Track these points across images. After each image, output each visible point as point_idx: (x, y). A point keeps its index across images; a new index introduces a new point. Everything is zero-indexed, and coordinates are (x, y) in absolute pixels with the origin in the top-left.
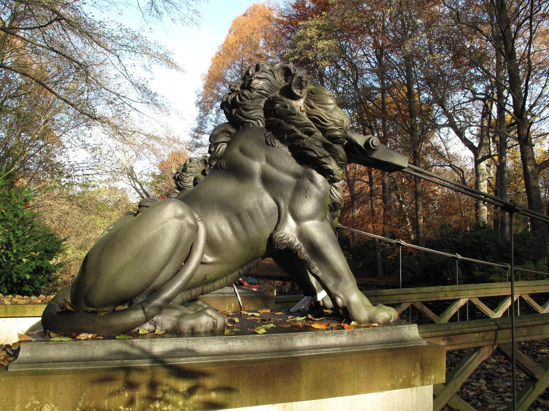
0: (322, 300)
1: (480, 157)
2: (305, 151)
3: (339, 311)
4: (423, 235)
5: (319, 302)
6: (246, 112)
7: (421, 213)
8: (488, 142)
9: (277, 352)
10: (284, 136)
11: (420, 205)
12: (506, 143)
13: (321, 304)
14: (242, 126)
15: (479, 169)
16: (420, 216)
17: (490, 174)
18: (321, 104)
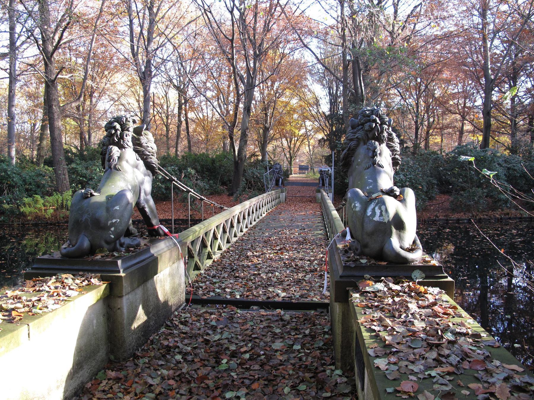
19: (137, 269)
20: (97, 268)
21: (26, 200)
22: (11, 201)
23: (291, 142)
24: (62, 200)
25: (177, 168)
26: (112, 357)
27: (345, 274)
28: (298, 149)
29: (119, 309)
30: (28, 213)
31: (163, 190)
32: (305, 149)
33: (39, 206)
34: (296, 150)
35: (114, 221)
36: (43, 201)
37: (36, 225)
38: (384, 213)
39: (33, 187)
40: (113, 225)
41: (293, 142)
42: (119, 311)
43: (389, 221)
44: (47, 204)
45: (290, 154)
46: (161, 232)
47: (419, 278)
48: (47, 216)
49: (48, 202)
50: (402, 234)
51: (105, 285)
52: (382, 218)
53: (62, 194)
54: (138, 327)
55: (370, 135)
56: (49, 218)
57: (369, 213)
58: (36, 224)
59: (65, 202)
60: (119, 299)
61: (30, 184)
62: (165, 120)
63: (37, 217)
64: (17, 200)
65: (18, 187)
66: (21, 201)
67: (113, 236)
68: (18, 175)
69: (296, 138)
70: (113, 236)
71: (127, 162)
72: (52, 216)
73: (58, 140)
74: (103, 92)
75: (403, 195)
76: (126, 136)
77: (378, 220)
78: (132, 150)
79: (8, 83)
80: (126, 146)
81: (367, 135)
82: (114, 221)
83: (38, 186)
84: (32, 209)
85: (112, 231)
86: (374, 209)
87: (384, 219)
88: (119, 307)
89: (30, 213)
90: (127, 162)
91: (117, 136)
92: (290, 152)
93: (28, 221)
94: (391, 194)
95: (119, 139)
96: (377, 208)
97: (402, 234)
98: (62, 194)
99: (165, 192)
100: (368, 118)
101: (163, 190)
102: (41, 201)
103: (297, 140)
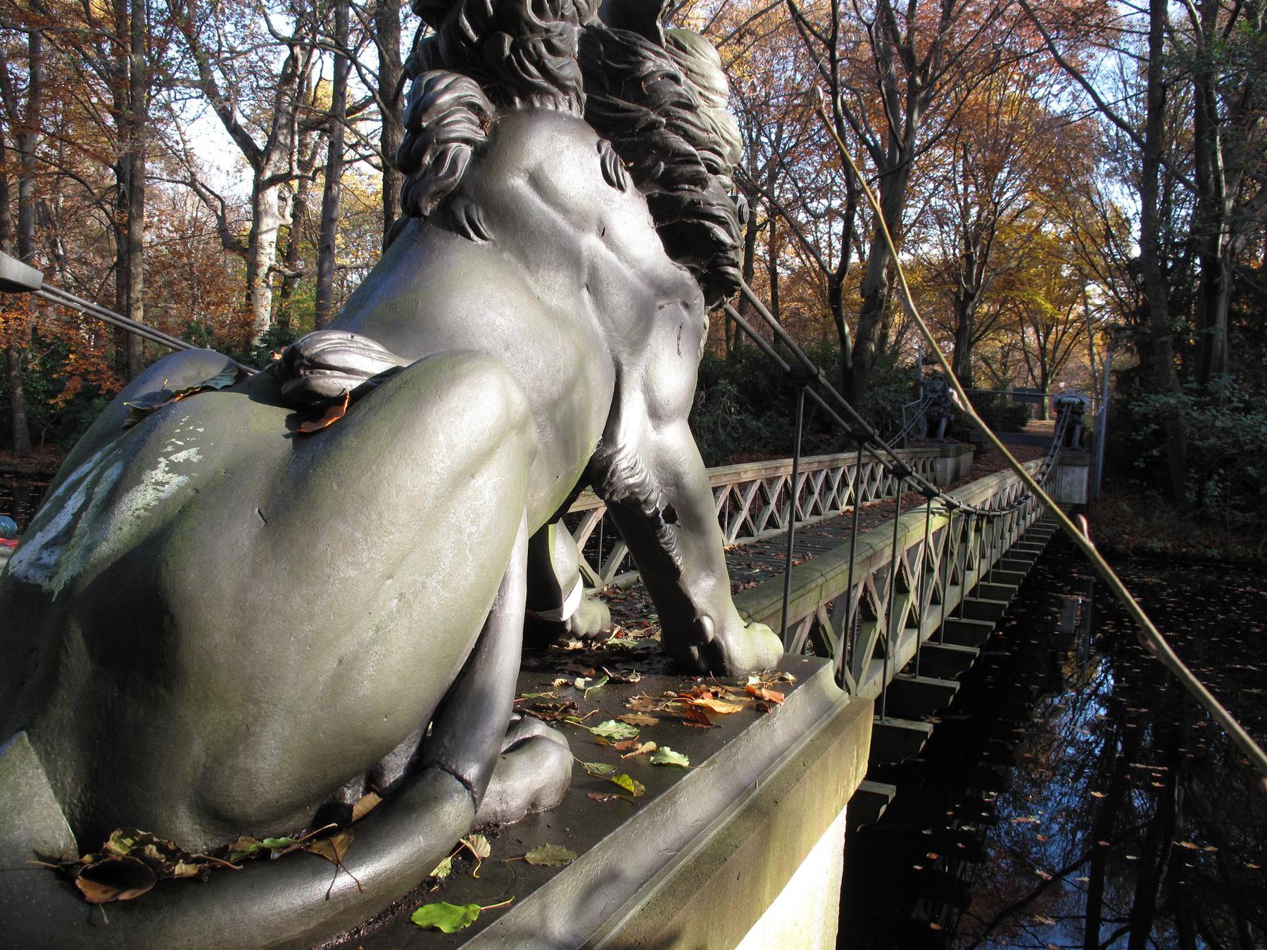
0: (572, 618)
1: (268, 174)
2: (707, 223)
3: (690, 650)
4: (141, 349)
5: (564, 623)
6: (549, 56)
7: (140, 296)
8: (288, 141)
9: (727, 806)
10: (656, 164)
11: (138, 275)
12: (342, 156)
13: (569, 627)
14: (523, 99)
15: (262, 202)
16: (137, 301)
17: (283, 217)
18: (704, 87)
23: (1046, 337)
28: (1067, 352)
34: (1058, 355)
41: (1052, 337)
69: (1060, 328)
103: (1064, 332)
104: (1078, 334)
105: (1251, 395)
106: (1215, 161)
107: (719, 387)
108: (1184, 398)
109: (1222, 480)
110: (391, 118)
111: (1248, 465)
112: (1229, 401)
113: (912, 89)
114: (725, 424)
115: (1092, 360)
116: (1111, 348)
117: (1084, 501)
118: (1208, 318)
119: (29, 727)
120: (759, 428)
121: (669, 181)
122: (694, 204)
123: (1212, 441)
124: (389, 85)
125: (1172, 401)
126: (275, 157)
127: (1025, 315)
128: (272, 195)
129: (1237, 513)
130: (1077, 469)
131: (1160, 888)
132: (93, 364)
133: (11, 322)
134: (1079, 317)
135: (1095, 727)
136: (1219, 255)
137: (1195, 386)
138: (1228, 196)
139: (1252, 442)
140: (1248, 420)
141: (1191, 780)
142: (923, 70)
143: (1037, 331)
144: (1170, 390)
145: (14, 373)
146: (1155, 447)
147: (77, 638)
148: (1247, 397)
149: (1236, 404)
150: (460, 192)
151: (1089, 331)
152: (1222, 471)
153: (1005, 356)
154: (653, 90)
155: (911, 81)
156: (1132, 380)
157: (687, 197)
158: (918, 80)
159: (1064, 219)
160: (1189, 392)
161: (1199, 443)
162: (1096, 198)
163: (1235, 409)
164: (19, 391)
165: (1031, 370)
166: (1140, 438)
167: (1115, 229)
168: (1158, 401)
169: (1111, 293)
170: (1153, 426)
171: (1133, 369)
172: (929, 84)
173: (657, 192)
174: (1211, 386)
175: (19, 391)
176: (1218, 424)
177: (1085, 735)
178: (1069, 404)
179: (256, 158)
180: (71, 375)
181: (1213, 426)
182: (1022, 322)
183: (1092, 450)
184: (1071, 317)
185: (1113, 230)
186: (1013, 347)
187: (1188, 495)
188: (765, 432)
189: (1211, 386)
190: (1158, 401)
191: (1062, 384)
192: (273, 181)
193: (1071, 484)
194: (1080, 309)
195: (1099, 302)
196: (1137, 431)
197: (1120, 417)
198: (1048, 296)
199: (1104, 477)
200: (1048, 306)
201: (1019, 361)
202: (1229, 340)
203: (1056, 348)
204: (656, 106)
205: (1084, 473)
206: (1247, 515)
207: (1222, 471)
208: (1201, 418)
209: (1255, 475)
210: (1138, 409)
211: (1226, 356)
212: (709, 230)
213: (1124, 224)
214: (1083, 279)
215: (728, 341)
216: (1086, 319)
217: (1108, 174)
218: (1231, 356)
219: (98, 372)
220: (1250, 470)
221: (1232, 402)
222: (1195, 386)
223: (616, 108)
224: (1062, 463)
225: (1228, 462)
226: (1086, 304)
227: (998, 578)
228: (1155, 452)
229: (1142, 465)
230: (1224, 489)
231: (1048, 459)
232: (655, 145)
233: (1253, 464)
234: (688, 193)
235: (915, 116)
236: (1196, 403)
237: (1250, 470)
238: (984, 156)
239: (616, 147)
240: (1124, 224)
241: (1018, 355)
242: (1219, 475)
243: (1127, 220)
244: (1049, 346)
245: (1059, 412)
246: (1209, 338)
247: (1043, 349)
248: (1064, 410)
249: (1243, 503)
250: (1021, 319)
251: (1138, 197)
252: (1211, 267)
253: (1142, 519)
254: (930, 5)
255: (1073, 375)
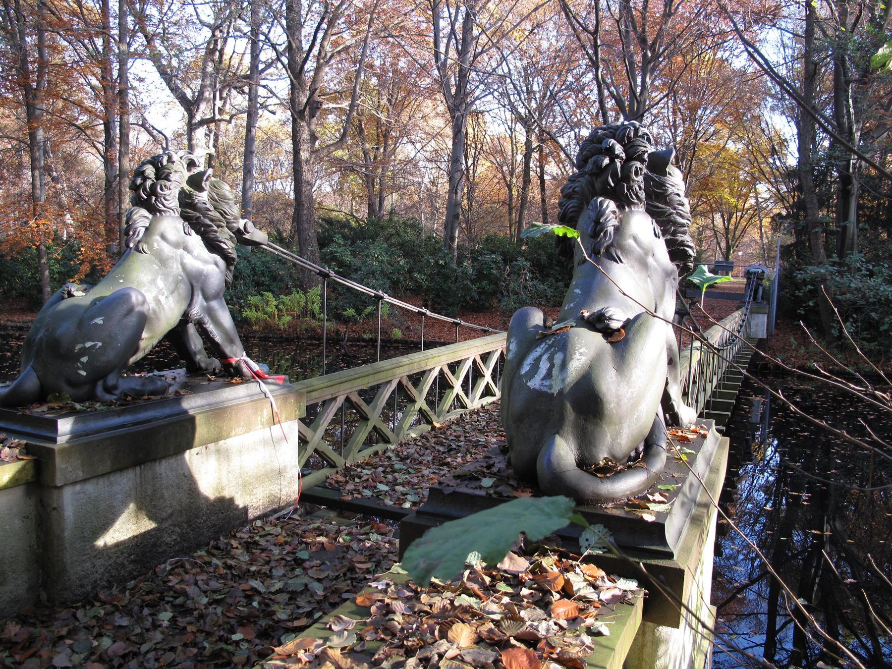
1: (198, 118)
19: (111, 438)
20: (28, 430)
21: (254, 299)
22: (232, 299)
23: (729, 220)
24: (306, 302)
25: (500, 258)
26: (44, 596)
27: (429, 509)
28: (744, 231)
29: (54, 509)
30: (253, 320)
31: (474, 294)
32: (753, 234)
33: (269, 310)
34: (738, 233)
35: (89, 344)
36: (275, 303)
37: (265, 339)
38: (555, 371)
39: (266, 279)
40: (84, 351)
41: (733, 220)
42: (54, 513)
43: (561, 392)
44: (281, 307)
45: (727, 242)
46: (245, 369)
47: (593, 548)
48: (282, 327)
49: (283, 303)
50: (590, 427)
51: (21, 463)
52: (547, 383)
53: (305, 292)
54: (117, 545)
55: (598, 185)
56: (285, 330)
57: (526, 368)
58: (265, 337)
59: (310, 305)
60: (56, 492)
61: (263, 274)
62: (508, 179)
63: (267, 327)
64: (240, 298)
65: (244, 278)
66: (246, 300)
67: (83, 373)
68: (245, 259)
69: (739, 214)
70: (83, 373)
71: (163, 237)
72: (290, 327)
73: (306, 206)
74: (405, 132)
75: (627, 334)
76: (162, 189)
77: (537, 387)
78: (177, 215)
79: (246, 119)
80: (162, 208)
81: (593, 186)
82: (89, 344)
83: (274, 278)
84: (260, 314)
85: (82, 363)
86: (538, 360)
87: (550, 387)
88: (55, 505)
89: (258, 320)
90: (163, 237)
91: (145, 190)
92: (727, 238)
93: (255, 332)
94: (599, 326)
95: (149, 197)
96: (545, 357)
97: (590, 427)
98: (305, 292)
99: (477, 297)
100: (598, 146)
101: (474, 294)
102: (273, 302)
103: (741, 217)
104: (751, 218)
105: (874, 266)
106: (848, 107)
107: (519, 263)
108: (830, 268)
109: (855, 321)
110: (297, 86)
111: (872, 311)
112: (859, 270)
113: (646, 60)
114: (525, 287)
115: (761, 237)
116: (775, 229)
117: (765, 337)
118: (844, 214)
119: (558, 433)
120: (545, 290)
121: (674, 233)
122: (682, 241)
123: (848, 296)
124: (295, 62)
125: (822, 271)
126: (203, 106)
127: (714, 205)
128: (200, 133)
129: (865, 343)
130: (760, 316)
131: (815, 589)
132: (97, 254)
133: (42, 227)
134: (751, 207)
135: (766, 489)
136: (851, 170)
137: (837, 260)
138: (857, 130)
139: (874, 296)
140: (872, 282)
141: (834, 520)
142: (652, 47)
143: (722, 216)
144: (820, 263)
145: (43, 261)
146: (810, 300)
147: (568, 406)
148: (871, 267)
149: (864, 272)
150: (611, 245)
151: (759, 217)
152: (855, 316)
153: (700, 234)
154: (671, 200)
155: (645, 56)
156: (791, 252)
157: (680, 239)
158: (649, 54)
159: (740, 139)
160: (834, 264)
161: (840, 297)
162: (763, 125)
163: (865, 276)
164: (47, 273)
165: (718, 243)
166: (801, 294)
167: (777, 148)
168: (812, 270)
169: (773, 190)
170: (809, 287)
171: (792, 245)
172: (656, 56)
173: (669, 237)
174: (847, 260)
175: (47, 273)
176: (852, 285)
177: (761, 496)
178: (755, 273)
179: (190, 106)
180: (83, 262)
181: (849, 286)
182: (712, 211)
183: (769, 303)
184: (747, 206)
185: (777, 148)
186: (705, 227)
187: (833, 331)
188: (550, 292)
189: (847, 260)
190: (812, 270)
191: (740, 253)
192: (203, 122)
193: (757, 326)
194: (752, 201)
195: (767, 196)
196: (799, 290)
197: (787, 279)
198: (731, 193)
199: (777, 318)
200: (733, 201)
201: (710, 237)
202: (857, 227)
203: (736, 228)
204: (668, 203)
205: (765, 317)
206: (872, 344)
207: (855, 316)
208: (842, 281)
209: (876, 318)
210: (799, 276)
211: (856, 237)
212: (687, 251)
213: (783, 143)
214: (755, 180)
215: (510, 227)
216: (758, 208)
217: (773, 109)
218: (858, 236)
219: (100, 260)
220: (873, 314)
221: (861, 270)
222: (837, 260)
223: (658, 207)
224: (751, 312)
225: (859, 310)
226: (756, 198)
227: (726, 387)
228: (811, 303)
229: (803, 312)
230: (857, 327)
231: (744, 309)
232: (672, 221)
233: (876, 311)
234: (680, 238)
235: (647, 79)
236: (838, 272)
237: (873, 314)
238: (688, 99)
239: (657, 222)
240: (783, 143)
241: (708, 233)
242: (853, 318)
243: (786, 140)
244: (731, 227)
245: (748, 279)
246: (845, 228)
247: (727, 229)
248: (752, 277)
249: (869, 336)
250: (712, 208)
251: (792, 124)
252: (846, 180)
253: (803, 348)
254: (657, 7)
255: (748, 246)
